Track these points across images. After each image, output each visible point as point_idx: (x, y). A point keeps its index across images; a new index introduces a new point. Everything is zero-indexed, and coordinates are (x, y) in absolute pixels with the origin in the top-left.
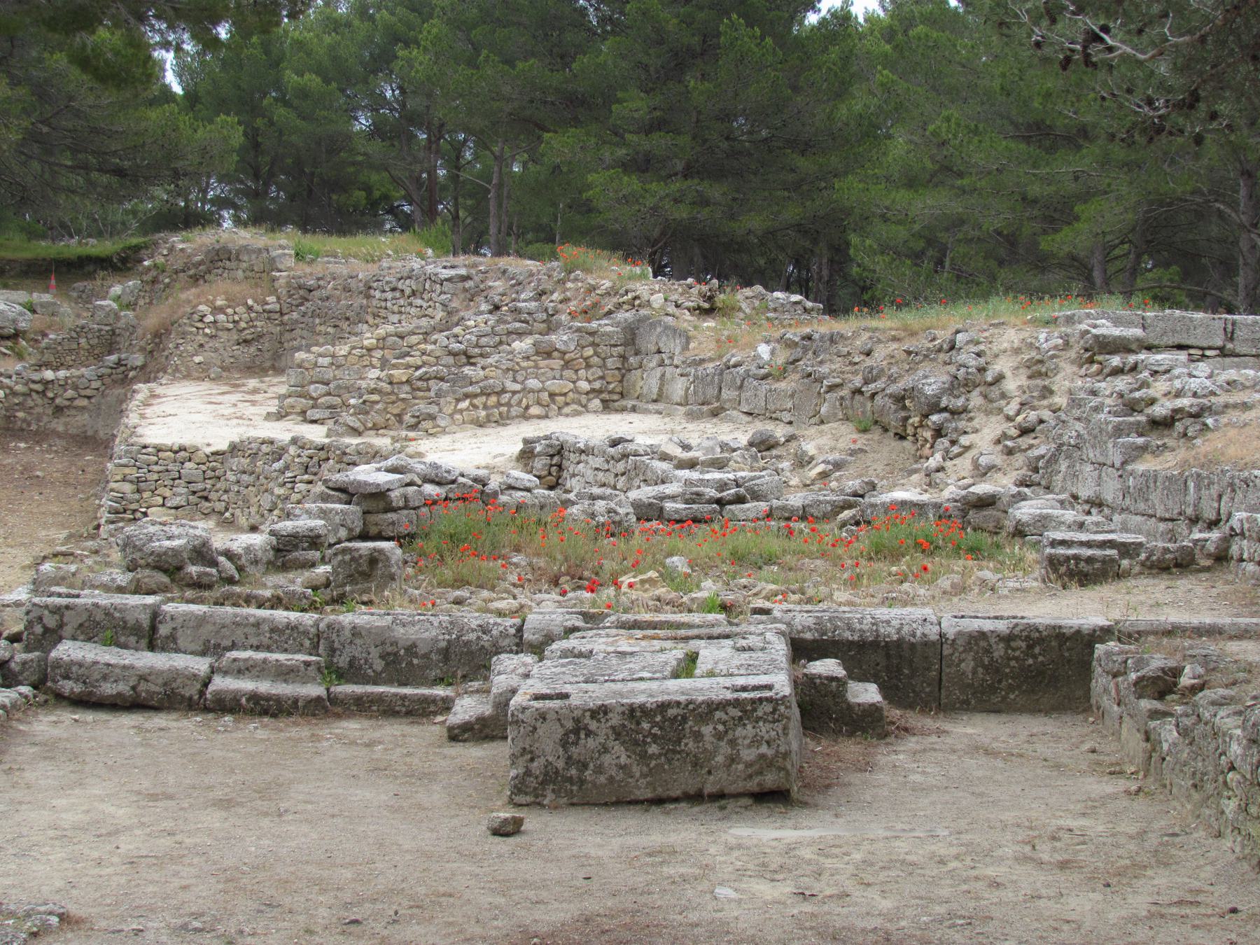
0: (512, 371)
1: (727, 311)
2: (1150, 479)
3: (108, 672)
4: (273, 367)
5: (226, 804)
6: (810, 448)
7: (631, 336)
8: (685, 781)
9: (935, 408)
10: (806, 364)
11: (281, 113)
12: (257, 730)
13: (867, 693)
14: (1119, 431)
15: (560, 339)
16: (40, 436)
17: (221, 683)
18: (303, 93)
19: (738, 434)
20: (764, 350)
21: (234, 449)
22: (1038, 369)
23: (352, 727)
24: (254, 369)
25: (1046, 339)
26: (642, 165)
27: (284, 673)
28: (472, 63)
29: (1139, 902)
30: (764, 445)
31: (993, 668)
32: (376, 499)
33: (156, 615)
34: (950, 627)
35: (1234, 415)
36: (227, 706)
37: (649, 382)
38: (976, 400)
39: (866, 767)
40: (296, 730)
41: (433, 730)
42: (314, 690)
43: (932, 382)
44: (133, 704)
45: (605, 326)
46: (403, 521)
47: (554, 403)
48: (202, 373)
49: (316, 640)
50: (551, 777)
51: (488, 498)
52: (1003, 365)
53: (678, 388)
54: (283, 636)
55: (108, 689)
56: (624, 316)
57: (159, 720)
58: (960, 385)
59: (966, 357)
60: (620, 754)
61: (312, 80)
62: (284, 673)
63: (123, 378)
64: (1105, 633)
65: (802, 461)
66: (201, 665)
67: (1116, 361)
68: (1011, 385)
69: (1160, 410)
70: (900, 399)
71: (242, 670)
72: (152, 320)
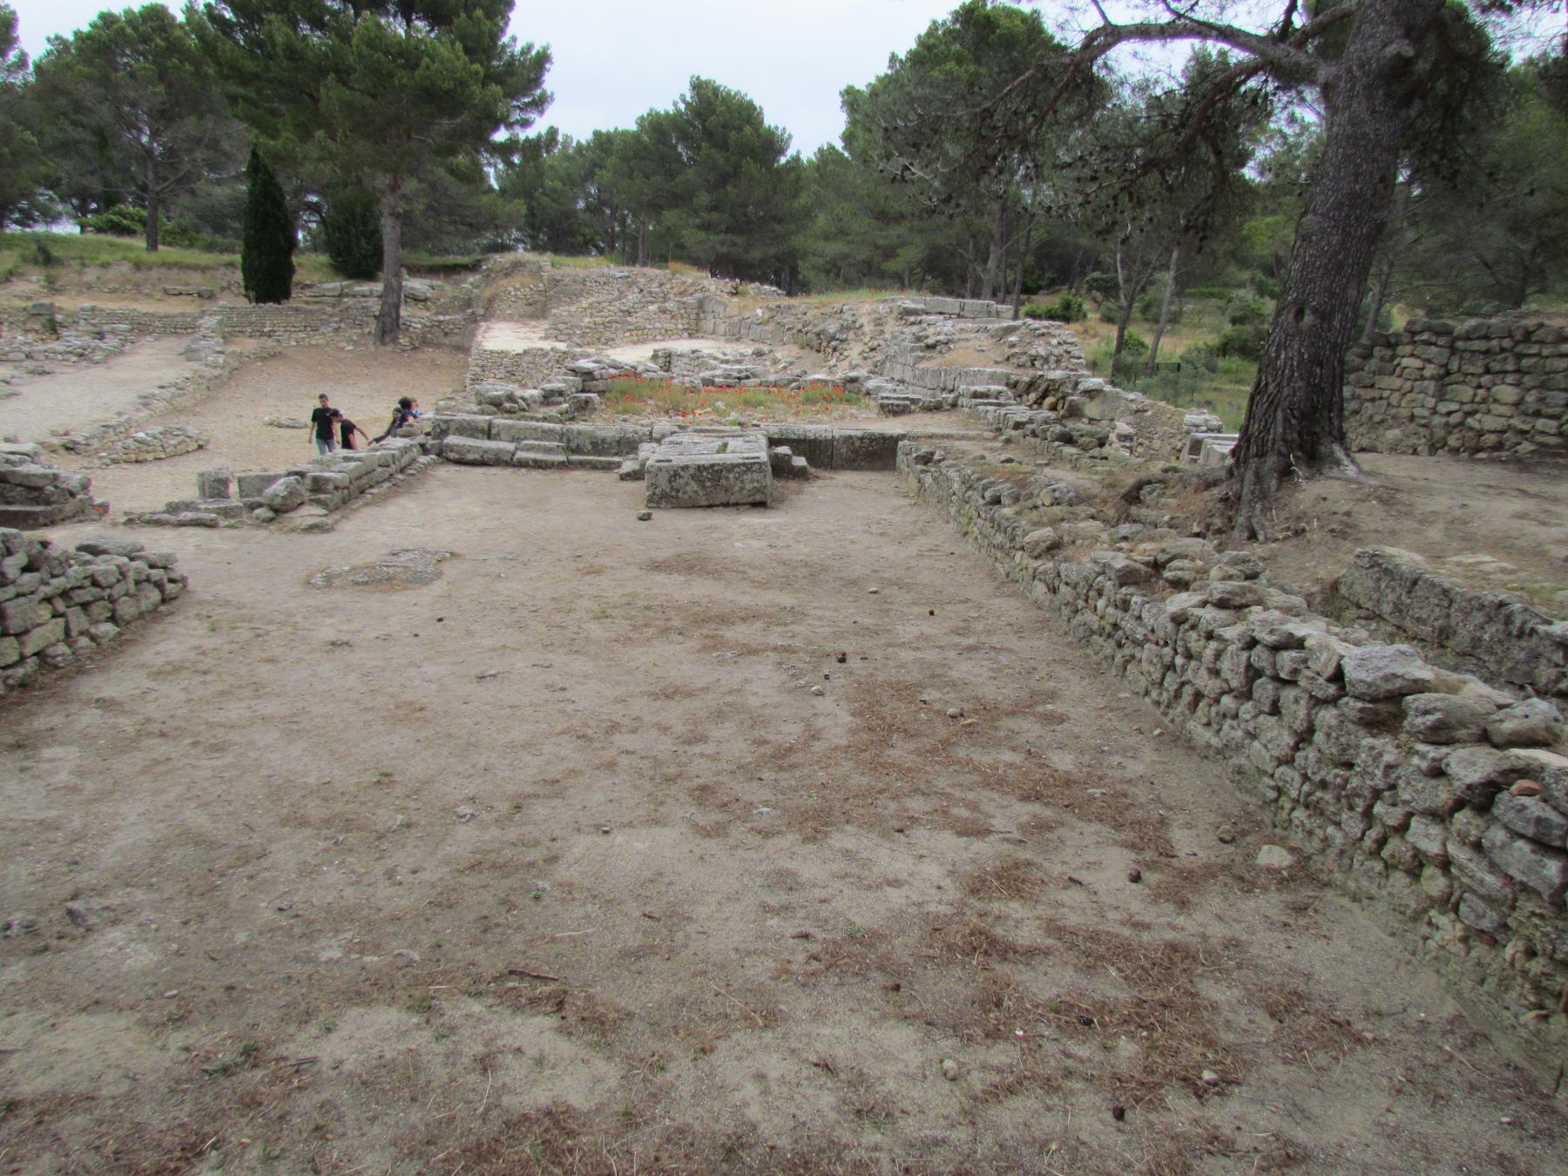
2: (925, 371)
3: (470, 449)
5: (522, 506)
6: (779, 355)
7: (701, 305)
9: (833, 338)
10: (778, 318)
12: (537, 475)
13: (800, 461)
14: (912, 350)
16: (438, 346)
17: (520, 455)
19: (747, 349)
20: (759, 312)
21: (526, 352)
22: (879, 322)
23: (578, 474)
25: (882, 309)
26: (707, 227)
27: (549, 450)
28: (630, 177)
30: (759, 354)
31: (855, 452)
33: (490, 425)
35: (962, 344)
36: (522, 464)
37: (708, 325)
38: (851, 335)
40: (553, 476)
42: (562, 458)
43: (832, 327)
45: (690, 300)
47: (667, 334)
49: (562, 436)
52: (863, 320)
53: (722, 328)
54: (547, 434)
55: (470, 457)
56: (699, 295)
57: (493, 470)
58: (844, 329)
60: (694, 486)
62: (549, 450)
63: (474, 320)
64: (903, 437)
65: (775, 362)
66: (511, 447)
67: (912, 319)
68: (867, 329)
69: (931, 341)
70: (818, 335)
71: (530, 449)
72: (487, 294)
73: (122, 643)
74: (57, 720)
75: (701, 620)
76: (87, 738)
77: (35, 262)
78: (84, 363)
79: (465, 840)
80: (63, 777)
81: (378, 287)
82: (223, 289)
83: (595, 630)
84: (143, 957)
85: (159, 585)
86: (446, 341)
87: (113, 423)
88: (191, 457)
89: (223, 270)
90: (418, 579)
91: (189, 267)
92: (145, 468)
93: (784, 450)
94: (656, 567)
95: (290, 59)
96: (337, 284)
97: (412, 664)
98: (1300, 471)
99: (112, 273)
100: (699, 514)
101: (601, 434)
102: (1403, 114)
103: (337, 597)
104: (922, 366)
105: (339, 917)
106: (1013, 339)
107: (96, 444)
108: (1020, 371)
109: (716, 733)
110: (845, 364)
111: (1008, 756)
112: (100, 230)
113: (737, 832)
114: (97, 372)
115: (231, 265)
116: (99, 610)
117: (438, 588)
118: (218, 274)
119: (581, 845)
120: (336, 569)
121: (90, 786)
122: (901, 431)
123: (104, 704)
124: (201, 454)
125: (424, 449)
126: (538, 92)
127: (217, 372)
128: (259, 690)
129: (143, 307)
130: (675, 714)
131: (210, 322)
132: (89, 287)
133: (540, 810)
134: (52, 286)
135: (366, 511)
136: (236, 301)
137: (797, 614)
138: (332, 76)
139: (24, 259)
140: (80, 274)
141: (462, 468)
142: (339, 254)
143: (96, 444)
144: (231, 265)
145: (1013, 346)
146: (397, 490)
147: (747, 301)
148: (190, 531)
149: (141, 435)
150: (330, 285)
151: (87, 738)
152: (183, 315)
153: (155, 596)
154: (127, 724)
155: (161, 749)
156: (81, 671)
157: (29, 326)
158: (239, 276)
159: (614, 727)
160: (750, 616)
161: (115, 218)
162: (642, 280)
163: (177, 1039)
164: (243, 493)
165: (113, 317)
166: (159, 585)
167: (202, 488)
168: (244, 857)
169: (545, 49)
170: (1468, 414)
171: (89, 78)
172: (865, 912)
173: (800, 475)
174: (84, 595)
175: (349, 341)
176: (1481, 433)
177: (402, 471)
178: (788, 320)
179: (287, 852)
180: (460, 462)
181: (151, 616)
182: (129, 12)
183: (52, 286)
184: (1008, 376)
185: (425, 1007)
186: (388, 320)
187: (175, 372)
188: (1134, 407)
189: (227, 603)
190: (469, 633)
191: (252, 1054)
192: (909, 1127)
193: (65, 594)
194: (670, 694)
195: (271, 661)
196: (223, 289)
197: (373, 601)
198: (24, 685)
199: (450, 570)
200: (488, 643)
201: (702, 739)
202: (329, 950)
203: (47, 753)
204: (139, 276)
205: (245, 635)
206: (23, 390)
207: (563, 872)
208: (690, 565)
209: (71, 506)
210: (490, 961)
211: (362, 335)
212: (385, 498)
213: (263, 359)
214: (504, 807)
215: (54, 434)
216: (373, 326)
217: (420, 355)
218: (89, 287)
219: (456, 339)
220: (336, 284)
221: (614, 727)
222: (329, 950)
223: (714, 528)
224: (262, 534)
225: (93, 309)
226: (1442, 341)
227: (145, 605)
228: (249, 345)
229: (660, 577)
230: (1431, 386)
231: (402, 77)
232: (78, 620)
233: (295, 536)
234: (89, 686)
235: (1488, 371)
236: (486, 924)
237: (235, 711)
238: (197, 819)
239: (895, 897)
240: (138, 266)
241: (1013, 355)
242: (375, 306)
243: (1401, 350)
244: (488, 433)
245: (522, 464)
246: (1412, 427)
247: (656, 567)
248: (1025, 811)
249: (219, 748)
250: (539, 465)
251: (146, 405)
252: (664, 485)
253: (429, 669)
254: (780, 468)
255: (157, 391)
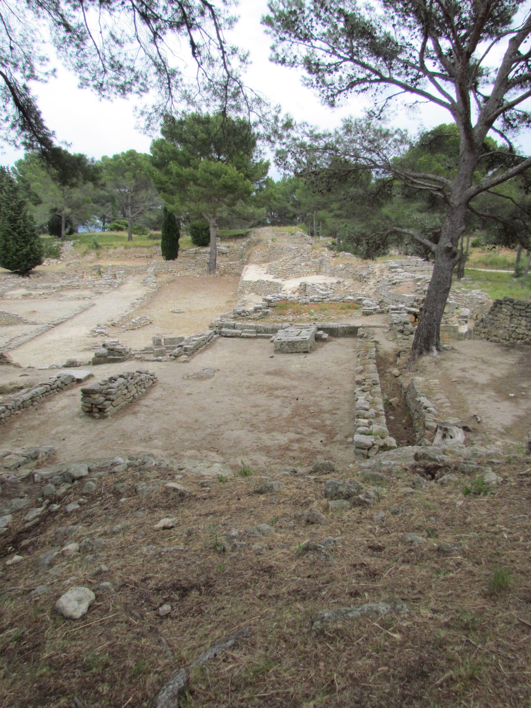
0: (301, 269)
1: (338, 256)
2: (390, 293)
3: (228, 333)
4: (390, 41)
5: (240, 353)
6: (346, 283)
7: (321, 262)
8: (295, 350)
9: (365, 278)
10: (347, 269)
11: (275, 202)
12: (247, 341)
13: (326, 336)
14: (387, 285)
15: (309, 263)
16: (230, 274)
17: (243, 334)
18: (279, 199)
19: (334, 280)
20: (341, 266)
21: (258, 281)
22: (382, 271)
23: (259, 340)
24: (265, 262)
25: (383, 266)
26: (337, 216)
27: (251, 332)
28: (306, 197)
29: (341, 368)
30: (339, 283)
31: (345, 332)
32: (270, 301)
33: (235, 325)
34: (340, 326)
35: (405, 283)
36: (243, 337)
37: (323, 269)
38: (371, 276)
39: (322, 347)
40: (252, 341)
41: (269, 340)
42: (255, 335)
43: (364, 273)
44: (232, 337)
45: (317, 260)
46: (274, 304)
47: (308, 274)
48: (255, 263)
49: (256, 328)
50: (279, 350)
51: (287, 300)
52: (376, 270)
53: (328, 271)
54: (251, 327)
55: (229, 335)
56: (320, 258)
57: (235, 339)
58: (369, 274)
59: (370, 269)
60: (287, 347)
61: (281, 196)
62: (251, 332)
63: (244, 264)
64: (360, 327)
65: (344, 286)
66: (240, 331)
67: (393, 270)
68: (377, 274)
69: (394, 282)
70: (360, 275)
71: (246, 332)
72: (248, 253)
73: (147, 393)
74: (139, 409)
75: (270, 389)
76: (145, 412)
77: (93, 248)
78: (111, 289)
79: (209, 431)
80: (142, 419)
81: (208, 249)
82: (154, 254)
83: (246, 391)
84: (160, 443)
85: (152, 380)
86: (233, 271)
87: (125, 315)
88: (148, 327)
89: (155, 247)
90: (209, 377)
91: (143, 247)
92: (135, 331)
93: (321, 332)
94: (268, 373)
95: (178, 177)
96: (194, 249)
97: (205, 399)
98: (424, 353)
99: (118, 250)
100: (288, 355)
101: (267, 327)
102: (452, 260)
103: (189, 382)
104: (389, 291)
105: (187, 440)
106: (419, 283)
107: (120, 323)
108: (420, 296)
109: (261, 414)
110: (368, 288)
111: (318, 421)
112: (112, 230)
113: (256, 431)
114: (116, 293)
115: (157, 245)
116: (142, 386)
117: (213, 379)
118: (153, 249)
119: (227, 433)
120: (190, 374)
121: (147, 420)
122: (360, 325)
123: (146, 406)
124: (151, 325)
125: (216, 333)
126: (266, 178)
127: (154, 290)
128: (174, 404)
129: (128, 264)
130: (254, 411)
131: (151, 270)
132: (110, 256)
133: (222, 427)
134: (98, 256)
135: (200, 355)
136: (159, 260)
137: (295, 387)
138: (192, 183)
139: (89, 247)
140: (107, 251)
141: (226, 338)
142: (195, 237)
143: (120, 323)
144: (157, 245)
145: (418, 286)
146: (207, 348)
147: (339, 259)
148: (156, 363)
149: (134, 320)
150: (192, 250)
151: (145, 412)
152: (142, 266)
153: (152, 382)
154: (151, 410)
155: (158, 414)
156: (140, 399)
157: (93, 273)
158: (160, 248)
159: (241, 413)
160: (284, 388)
161: (116, 224)
162: (302, 250)
163: (166, 452)
164: (165, 344)
165: (120, 268)
166: (152, 380)
167: (154, 342)
168: (173, 432)
169: (268, 161)
170: (517, 328)
171: (111, 180)
172: (269, 443)
173: (324, 340)
174: (140, 383)
175: (198, 273)
176: (519, 334)
177: (209, 341)
178: (351, 269)
179: (180, 431)
180: (226, 336)
181: (151, 387)
182: (123, 153)
183: (98, 256)
184: (415, 298)
185: (199, 450)
186: (212, 265)
187: (141, 292)
188: (480, 301)
189: (166, 384)
190: (217, 392)
191: (176, 454)
192: (259, 466)
193: (137, 383)
194: (255, 406)
195: (176, 397)
196: (154, 254)
197: (198, 383)
198: (131, 402)
199: (216, 374)
200: (221, 394)
201: (257, 415)
202: (186, 444)
203: (139, 415)
204: (126, 251)
205: (170, 391)
206: (95, 302)
207: (223, 436)
208: (277, 373)
209: (128, 355)
210: (209, 446)
211: (202, 271)
212: (203, 351)
213: (169, 283)
214: (216, 426)
215: (109, 321)
216: (206, 268)
217: (224, 278)
218: (110, 256)
219: (236, 271)
220: (194, 249)
221: (241, 413)
222: (186, 444)
223: (289, 361)
224: (172, 363)
225: (112, 266)
226: (511, 304)
227: (150, 384)
228: (165, 277)
229: (268, 377)
230: (508, 318)
231: (215, 182)
232: (139, 389)
233: (180, 364)
234: (143, 402)
235: (520, 315)
236: (209, 442)
237: (170, 408)
238: (166, 426)
239: (276, 442)
240: (126, 247)
241: (418, 290)
242: (207, 258)
243: (503, 306)
244: (234, 327)
245: (243, 337)
246: (505, 330)
247: (268, 373)
248: (311, 430)
249: (168, 415)
250: (248, 337)
251: (133, 307)
252: (279, 347)
253: (208, 400)
254: (318, 338)
255: (136, 301)
